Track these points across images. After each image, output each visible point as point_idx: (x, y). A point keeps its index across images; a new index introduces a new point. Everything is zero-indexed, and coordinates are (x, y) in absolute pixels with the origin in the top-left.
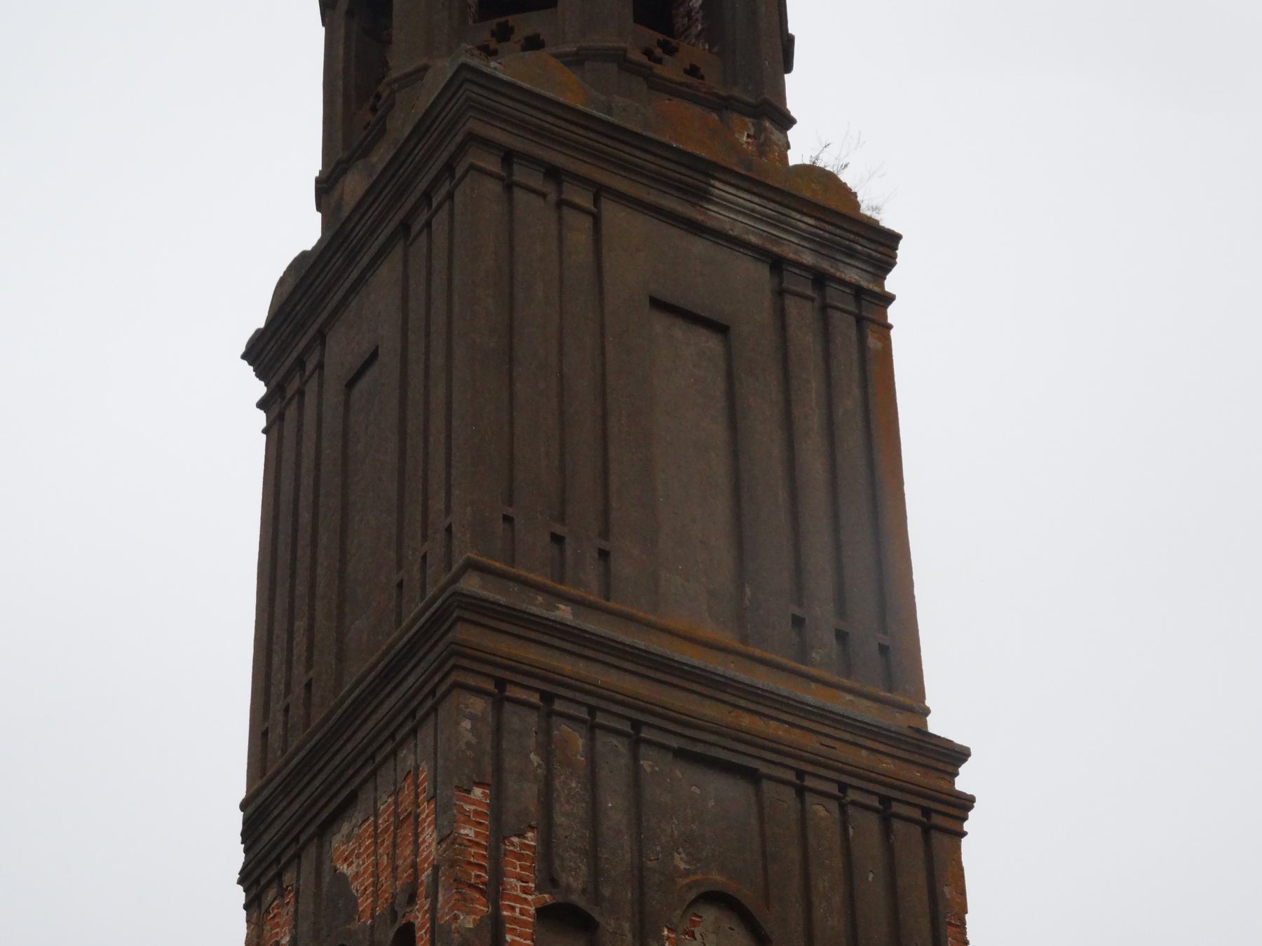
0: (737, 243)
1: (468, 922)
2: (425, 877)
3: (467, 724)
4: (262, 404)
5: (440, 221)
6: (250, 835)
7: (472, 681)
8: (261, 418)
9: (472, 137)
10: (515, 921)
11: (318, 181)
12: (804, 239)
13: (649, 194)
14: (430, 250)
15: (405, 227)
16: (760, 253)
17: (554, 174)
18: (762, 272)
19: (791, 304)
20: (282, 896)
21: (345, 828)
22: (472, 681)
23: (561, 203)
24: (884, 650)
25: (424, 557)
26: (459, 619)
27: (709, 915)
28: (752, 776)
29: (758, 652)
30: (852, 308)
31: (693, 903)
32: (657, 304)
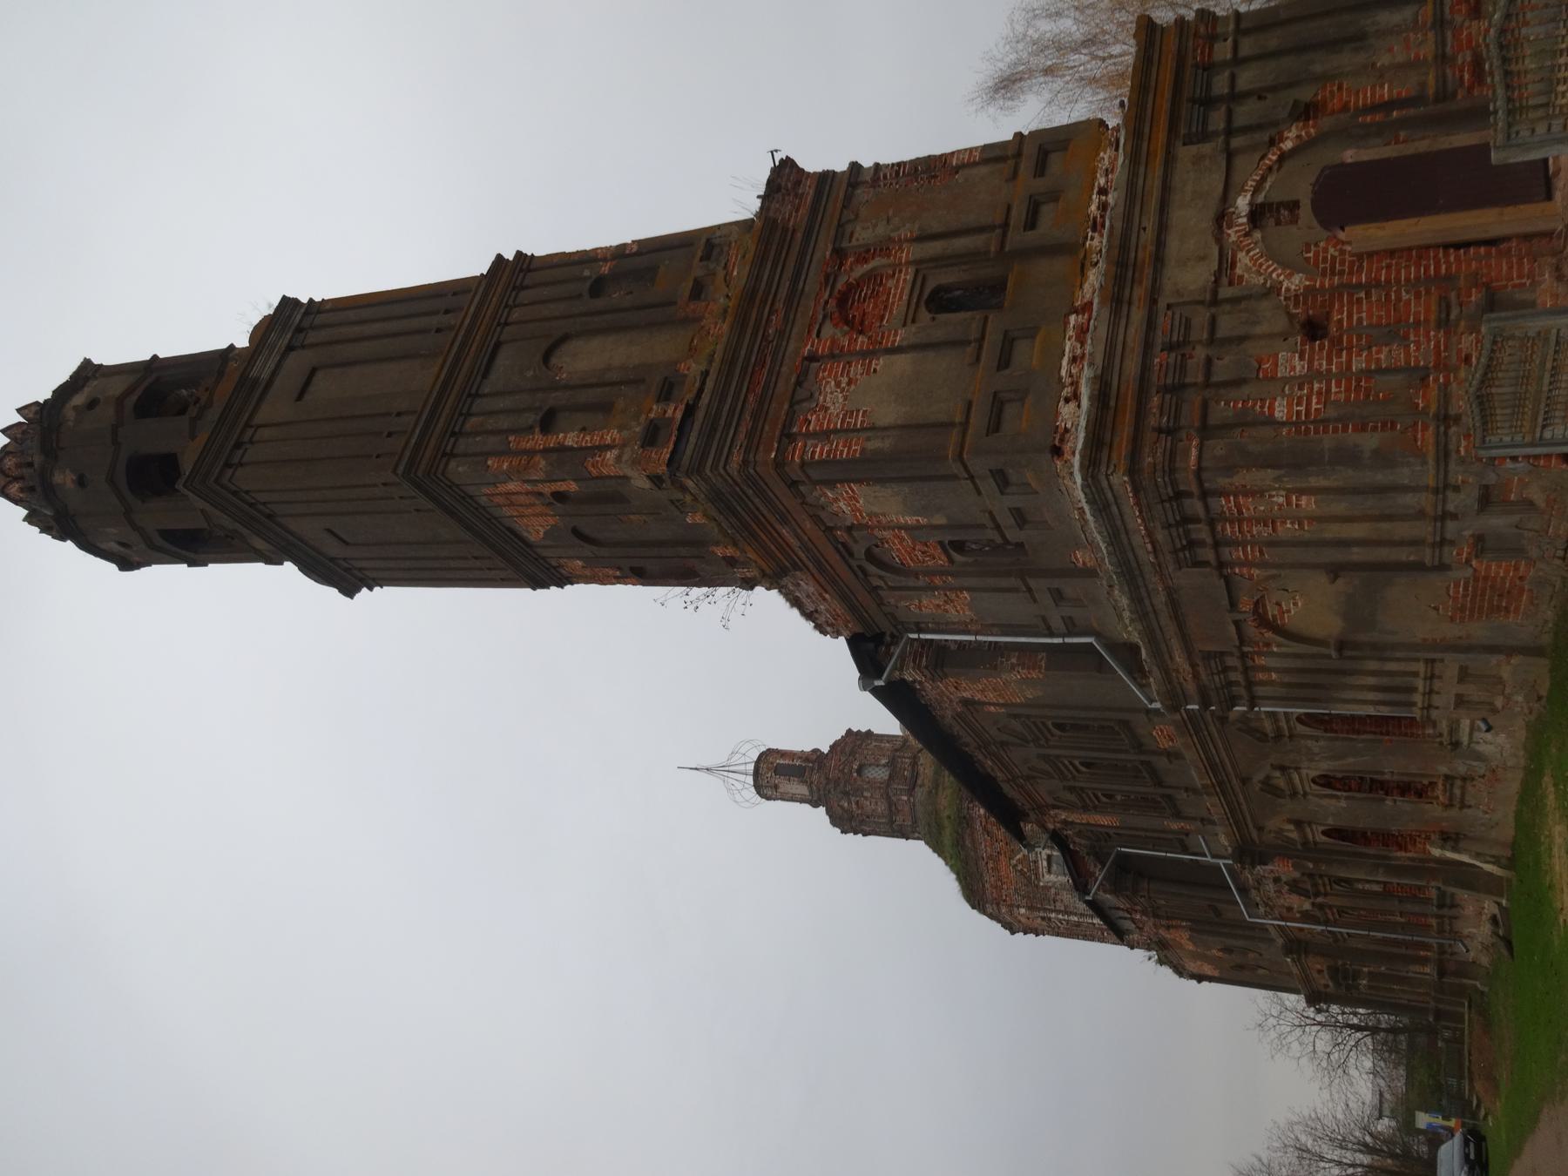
0: (279, 365)
1: (543, 463)
4: (371, 589)
6: (545, 585)
7: (442, 466)
8: (377, 589)
9: (217, 481)
10: (545, 443)
12: (281, 337)
15: (269, 517)
17: (238, 445)
18: (293, 354)
19: (307, 342)
20: (563, 566)
21: (525, 534)
22: (442, 466)
23: (251, 442)
25: (401, 498)
27: (554, 361)
28: (498, 345)
29: (447, 349)
30: (313, 316)
31: (547, 367)
32: (300, 397)
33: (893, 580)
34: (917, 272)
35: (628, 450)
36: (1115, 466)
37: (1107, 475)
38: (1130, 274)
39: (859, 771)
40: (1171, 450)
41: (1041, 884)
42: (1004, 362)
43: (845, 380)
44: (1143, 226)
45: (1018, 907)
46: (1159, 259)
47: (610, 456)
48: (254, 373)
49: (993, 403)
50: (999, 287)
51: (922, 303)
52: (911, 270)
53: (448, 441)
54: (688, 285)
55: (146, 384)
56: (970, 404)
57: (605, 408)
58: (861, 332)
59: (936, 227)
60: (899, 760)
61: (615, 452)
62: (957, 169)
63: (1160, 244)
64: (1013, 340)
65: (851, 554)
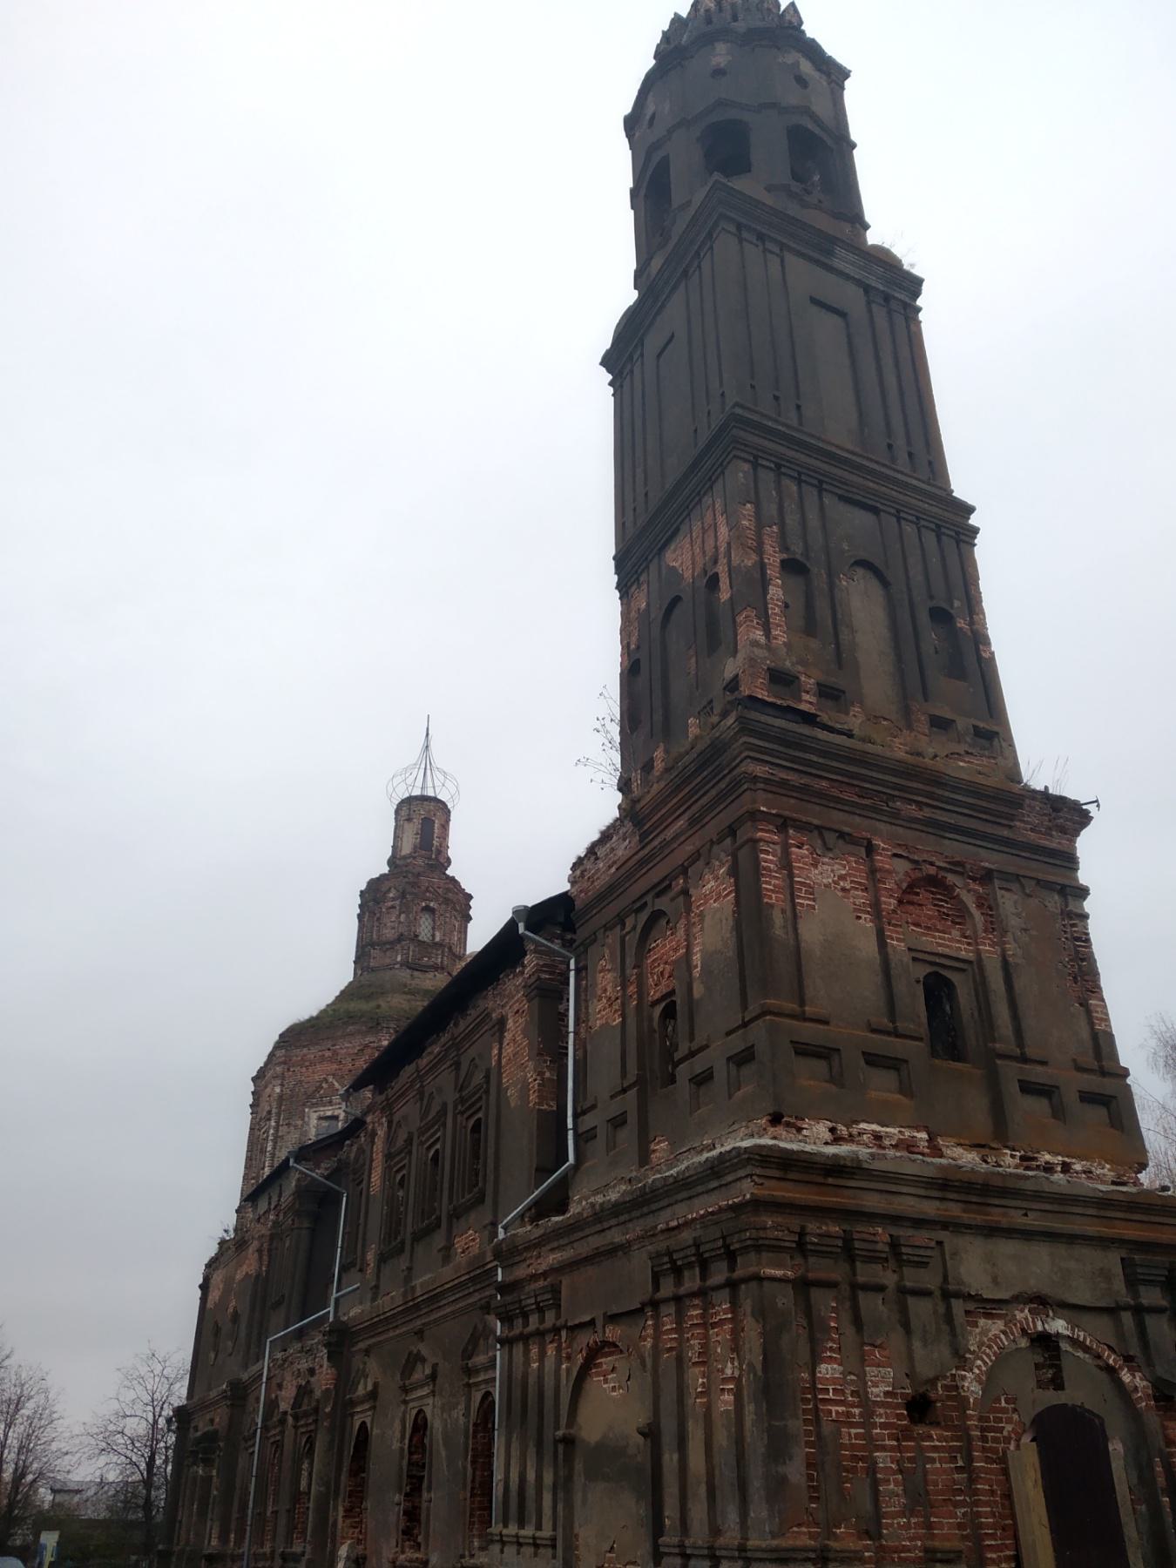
0: (848, 277)
2: (722, 549)
3: (741, 475)
4: (611, 384)
5: (706, 265)
6: (618, 570)
8: (611, 390)
10: (770, 564)
11: (636, 272)
13: (321, 1366)
14: (701, 282)
16: (859, 283)
22: (743, 455)
24: (930, 463)
26: (734, 426)
27: (860, 572)
28: (875, 511)
31: (853, 565)
32: (815, 301)
33: (632, 940)
34: (970, 962)
36: (762, 1184)
39: (427, 909)
40: (780, 1247)
41: (307, 1110)
42: (872, 1060)
45: (282, 1085)
46: (992, 1231)
47: (759, 635)
52: (971, 956)
53: (771, 461)
56: (826, 1023)
58: (900, 902)
59: (1019, 984)
60: (439, 952)
61: (763, 640)
62: (1084, 1004)
63: (1010, 1233)
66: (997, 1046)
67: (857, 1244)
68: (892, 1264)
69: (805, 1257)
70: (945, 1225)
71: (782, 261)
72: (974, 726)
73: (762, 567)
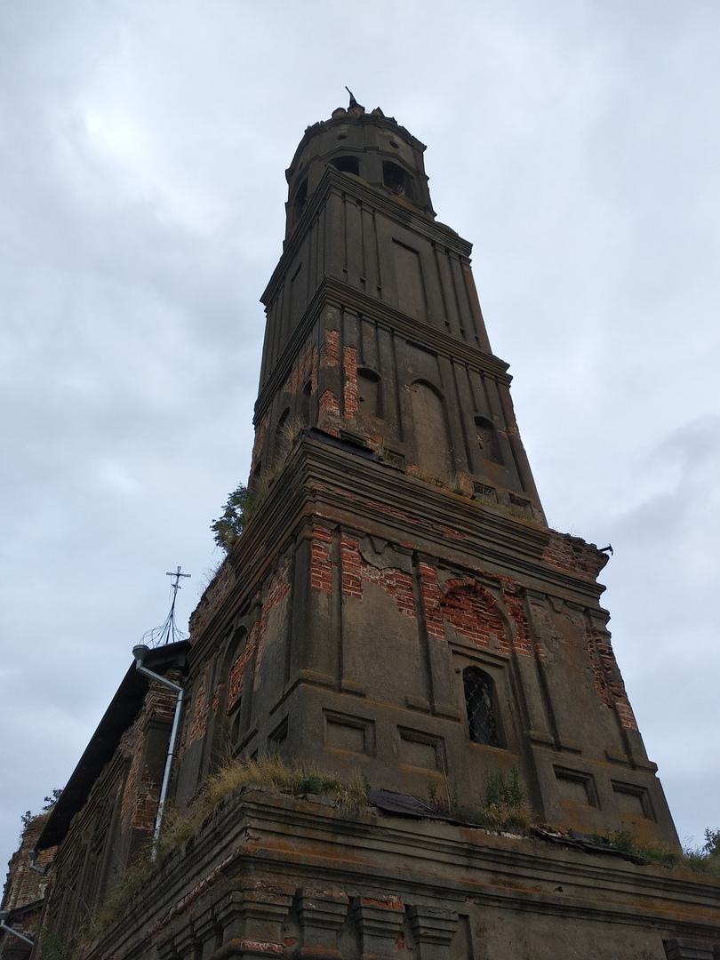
9: (310, 476)
16: (428, 239)
19: (438, 253)
27: (421, 388)
28: (434, 354)
33: (221, 661)
34: (507, 660)
35: (339, 421)
36: (257, 839)
37: (245, 829)
38: (505, 869)
40: (268, 913)
41: (40, 885)
42: (408, 734)
43: (393, 583)
44: (563, 887)
45: (25, 865)
46: (523, 905)
47: (335, 409)
48: (413, 219)
49: (362, 719)
50: (496, 739)
51: (473, 663)
52: (507, 655)
54: (488, 482)
55: (408, 171)
56: (362, 695)
57: (380, 412)
58: (443, 605)
59: (552, 681)
61: (338, 413)
62: (612, 706)
63: (543, 907)
64: (434, 747)
65: (242, 615)
66: (532, 732)
67: (365, 913)
68: (408, 942)
69: (301, 927)
70: (472, 894)
71: (374, 218)
72: (510, 494)
73: (342, 370)
